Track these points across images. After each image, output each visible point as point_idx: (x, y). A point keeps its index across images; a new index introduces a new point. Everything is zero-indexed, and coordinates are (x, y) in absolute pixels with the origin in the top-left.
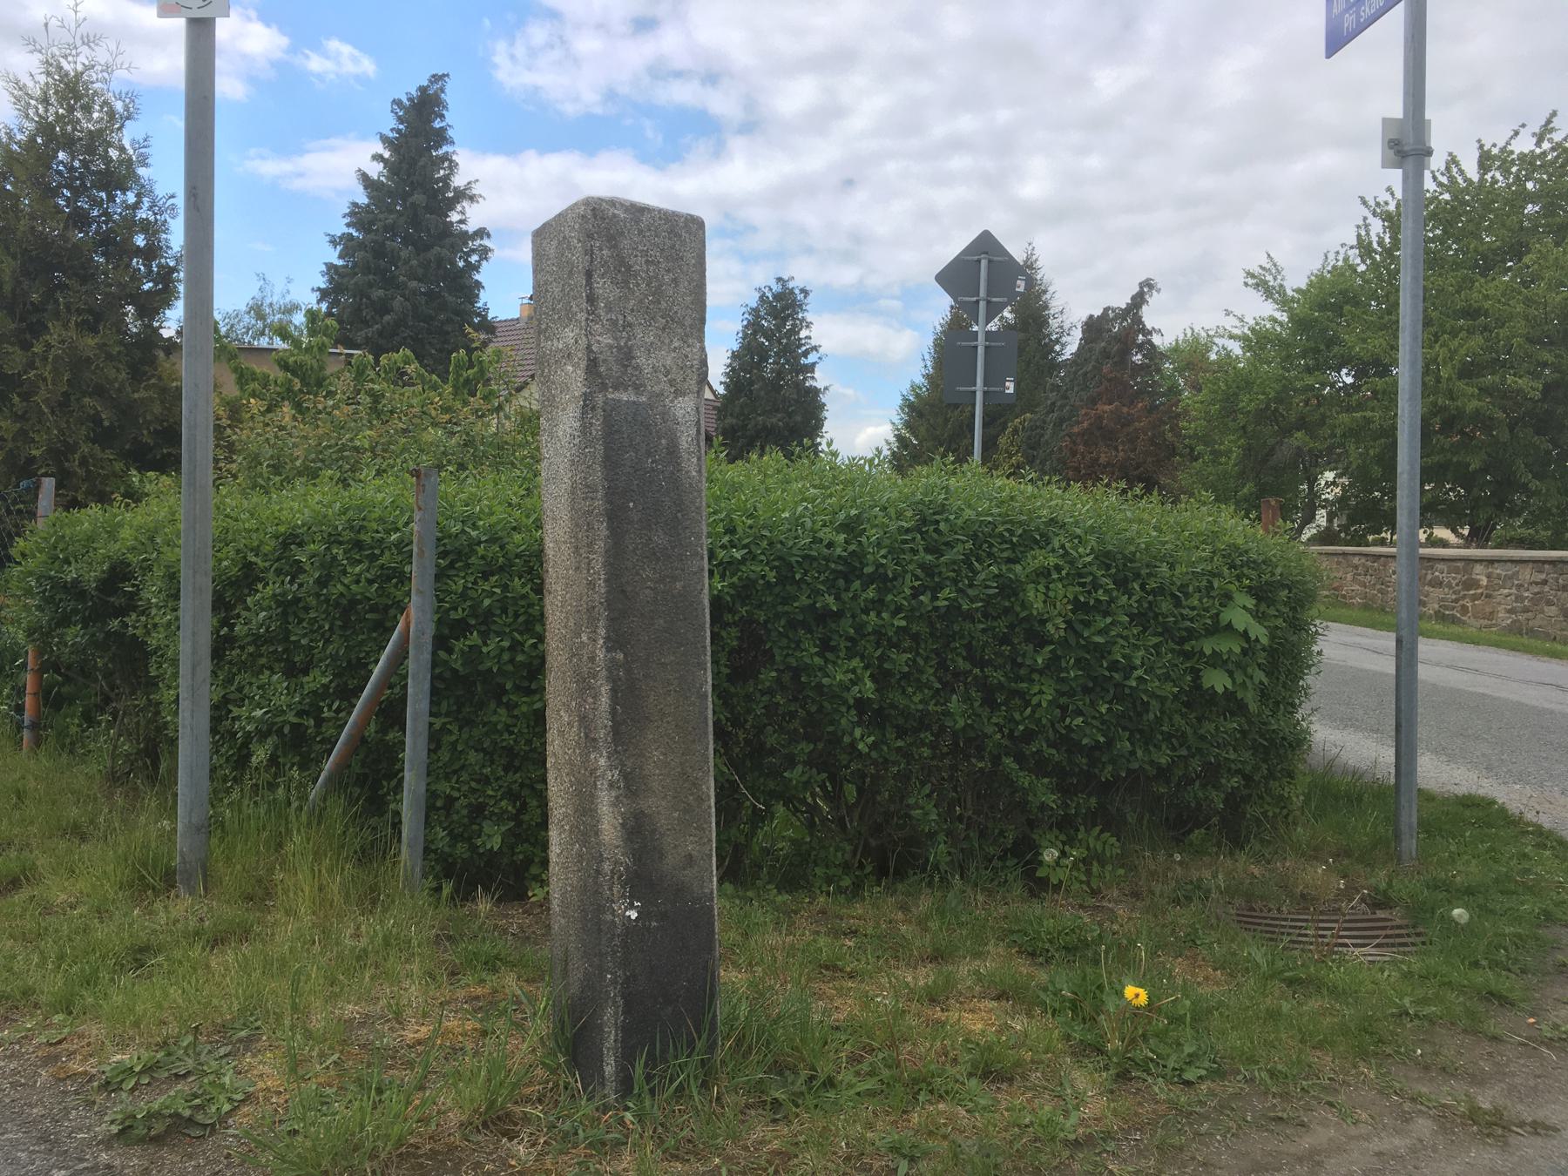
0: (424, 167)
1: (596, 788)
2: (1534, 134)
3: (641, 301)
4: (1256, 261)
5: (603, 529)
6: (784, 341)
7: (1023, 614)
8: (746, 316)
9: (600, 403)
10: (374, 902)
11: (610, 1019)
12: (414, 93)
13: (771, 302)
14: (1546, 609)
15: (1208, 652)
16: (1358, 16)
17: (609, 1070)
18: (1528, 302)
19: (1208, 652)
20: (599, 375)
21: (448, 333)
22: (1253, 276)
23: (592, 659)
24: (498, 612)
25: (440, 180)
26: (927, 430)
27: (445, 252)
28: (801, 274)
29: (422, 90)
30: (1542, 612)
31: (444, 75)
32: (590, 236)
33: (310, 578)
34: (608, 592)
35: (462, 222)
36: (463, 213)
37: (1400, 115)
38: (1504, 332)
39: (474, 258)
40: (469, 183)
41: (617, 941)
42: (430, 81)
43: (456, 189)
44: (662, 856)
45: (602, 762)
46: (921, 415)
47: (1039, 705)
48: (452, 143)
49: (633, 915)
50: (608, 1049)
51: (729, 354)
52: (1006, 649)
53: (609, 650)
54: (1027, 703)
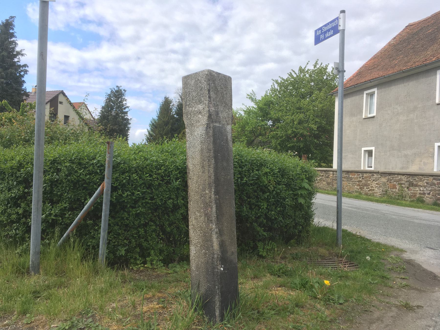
0: (6, 44)
1: (212, 234)
2: (313, 65)
3: (220, 99)
4: (250, 90)
5: (213, 161)
6: (118, 104)
7: (261, 184)
8: (107, 96)
9: (212, 126)
10: (97, 272)
11: (217, 299)
12: (4, 21)
13: (114, 93)
14: (323, 182)
15: (300, 194)
16: (325, 36)
17: (217, 313)
18: (314, 106)
19: (300, 194)
20: (212, 119)
21: (13, 96)
22: (249, 95)
23: (210, 198)
24: (127, 184)
25: (11, 48)
26: (158, 132)
27: (13, 71)
28: (123, 84)
29: (7, 20)
30: (322, 183)
31: (14, 17)
32: (209, 80)
33: (62, 174)
34: (215, 179)
35: (18, 62)
36: (19, 59)
37: (338, 62)
38: (308, 113)
39: (22, 73)
40: (22, 50)
41: (219, 277)
42: (10, 18)
43: (16, 52)
44: (227, 253)
45: (214, 226)
46: (156, 127)
47: (263, 208)
48: (16, 37)
49: (222, 269)
50: (217, 308)
51: (101, 107)
52: (256, 194)
53: (215, 195)
54: (260, 208)
